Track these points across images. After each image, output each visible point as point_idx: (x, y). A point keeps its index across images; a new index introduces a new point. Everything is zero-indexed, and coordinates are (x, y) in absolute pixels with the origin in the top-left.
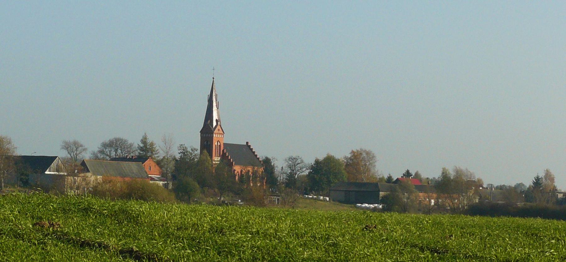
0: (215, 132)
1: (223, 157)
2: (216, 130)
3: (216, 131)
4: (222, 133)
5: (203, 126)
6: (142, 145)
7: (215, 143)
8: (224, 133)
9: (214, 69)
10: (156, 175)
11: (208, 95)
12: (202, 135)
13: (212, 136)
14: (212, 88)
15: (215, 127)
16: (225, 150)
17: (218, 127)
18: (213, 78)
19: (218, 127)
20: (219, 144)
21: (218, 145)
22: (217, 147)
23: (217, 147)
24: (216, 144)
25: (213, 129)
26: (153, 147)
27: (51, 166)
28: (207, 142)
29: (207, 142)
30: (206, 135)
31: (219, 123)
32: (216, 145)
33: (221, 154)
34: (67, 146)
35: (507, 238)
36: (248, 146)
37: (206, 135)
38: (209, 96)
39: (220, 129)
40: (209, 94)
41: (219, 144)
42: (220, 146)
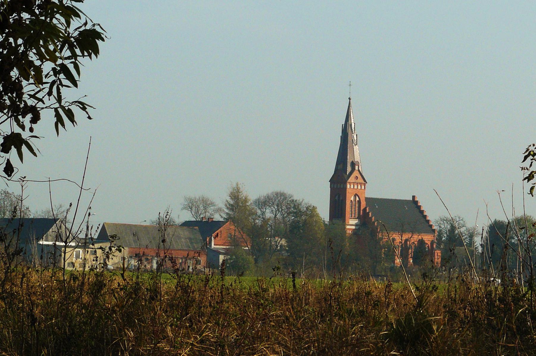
0: (349, 180)
1: (364, 218)
2: (351, 178)
3: (352, 179)
4: (364, 182)
5: (333, 173)
6: (232, 202)
7: (351, 198)
8: (367, 183)
9: (350, 85)
10: (219, 245)
11: (343, 125)
12: (332, 185)
13: (332, 185)
14: (58, 130)
15: (349, 174)
16: (367, 208)
17: (356, 173)
18: (350, 99)
19: (354, 173)
20: (357, 199)
21: (357, 201)
22: (354, 203)
23: (354, 203)
24: (352, 199)
25: (346, 177)
26: (247, 204)
27: (48, 232)
28: (339, 197)
29: (339, 197)
30: (340, 185)
31: (357, 168)
32: (351, 201)
33: (361, 214)
34: (191, 205)
35: (209, 299)
36: (414, 202)
37: (340, 185)
38: (344, 125)
39: (359, 176)
40: (344, 124)
41: (357, 199)
42: (359, 202)
